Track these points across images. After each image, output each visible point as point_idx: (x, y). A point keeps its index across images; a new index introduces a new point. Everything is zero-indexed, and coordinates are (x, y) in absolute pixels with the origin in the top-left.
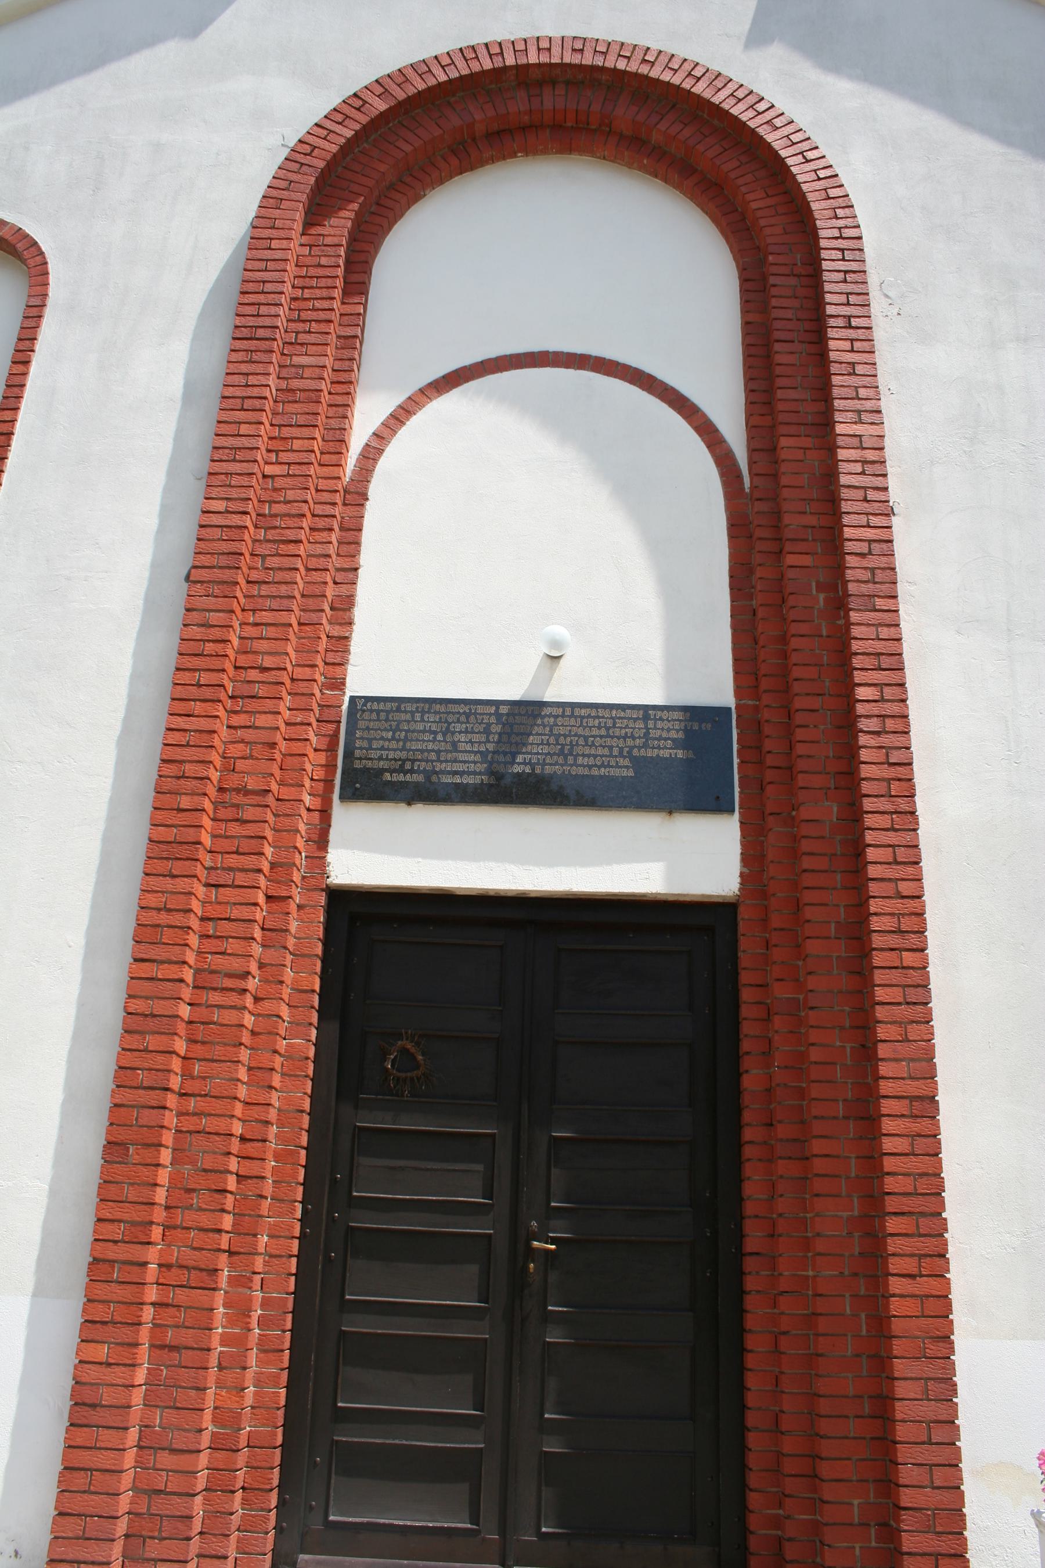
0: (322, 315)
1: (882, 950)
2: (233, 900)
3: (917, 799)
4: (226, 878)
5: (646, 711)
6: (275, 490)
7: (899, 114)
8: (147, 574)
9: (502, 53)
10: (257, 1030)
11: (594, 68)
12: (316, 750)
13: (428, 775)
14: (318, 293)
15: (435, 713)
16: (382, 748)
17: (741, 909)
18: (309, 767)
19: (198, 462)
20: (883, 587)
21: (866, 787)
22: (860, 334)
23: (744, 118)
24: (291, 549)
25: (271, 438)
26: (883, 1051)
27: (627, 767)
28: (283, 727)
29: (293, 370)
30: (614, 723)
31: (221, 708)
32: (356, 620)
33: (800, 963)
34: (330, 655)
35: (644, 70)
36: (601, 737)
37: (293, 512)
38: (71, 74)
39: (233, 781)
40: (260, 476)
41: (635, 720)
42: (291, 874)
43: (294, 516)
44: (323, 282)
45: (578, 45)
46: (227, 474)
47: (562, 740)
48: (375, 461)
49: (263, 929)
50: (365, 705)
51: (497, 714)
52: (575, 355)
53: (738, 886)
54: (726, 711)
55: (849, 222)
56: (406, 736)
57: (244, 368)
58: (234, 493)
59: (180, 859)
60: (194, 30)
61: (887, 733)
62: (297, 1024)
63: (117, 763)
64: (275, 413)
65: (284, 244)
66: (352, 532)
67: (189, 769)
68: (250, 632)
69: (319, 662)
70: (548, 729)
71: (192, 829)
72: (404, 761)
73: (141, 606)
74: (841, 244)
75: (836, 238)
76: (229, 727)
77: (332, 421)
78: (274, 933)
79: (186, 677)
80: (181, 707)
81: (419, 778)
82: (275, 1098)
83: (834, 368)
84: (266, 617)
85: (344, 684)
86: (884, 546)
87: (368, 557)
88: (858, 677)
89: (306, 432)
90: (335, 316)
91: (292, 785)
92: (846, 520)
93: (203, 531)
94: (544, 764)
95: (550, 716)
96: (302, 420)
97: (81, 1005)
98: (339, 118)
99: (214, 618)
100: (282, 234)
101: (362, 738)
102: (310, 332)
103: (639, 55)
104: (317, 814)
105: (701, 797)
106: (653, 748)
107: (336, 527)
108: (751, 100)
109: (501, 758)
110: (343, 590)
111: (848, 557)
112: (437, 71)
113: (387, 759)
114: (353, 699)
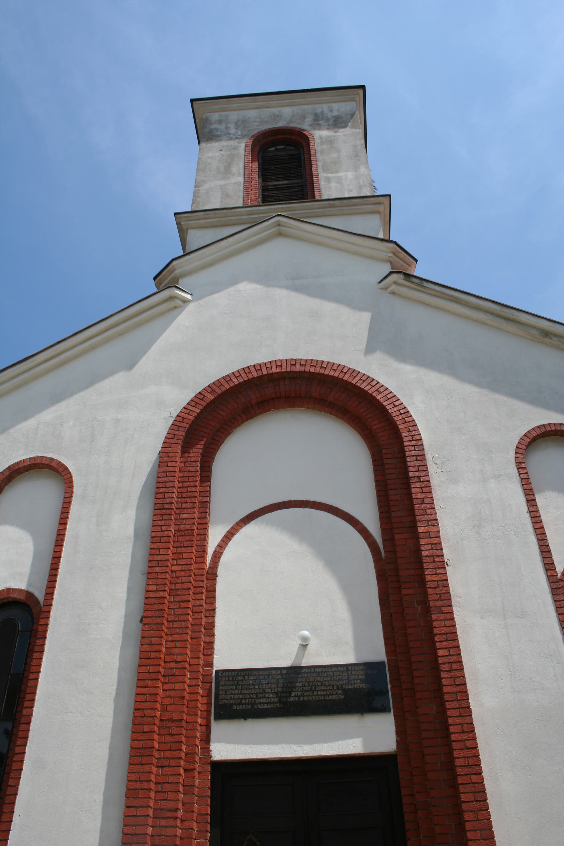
0: (192, 494)
1: (462, 775)
2: (169, 773)
3: (470, 700)
4: (166, 763)
5: (347, 667)
6: (177, 577)
7: (434, 379)
8: (123, 620)
9: (261, 369)
10: (183, 836)
11: (300, 372)
12: (202, 696)
13: (252, 705)
14: (189, 484)
15: (254, 675)
16: (232, 694)
17: (398, 758)
18: (199, 705)
19: (142, 566)
20: (445, 602)
21: (446, 697)
22: (425, 484)
23: (366, 389)
24: (186, 605)
25: (173, 553)
26: (468, 826)
27: (341, 694)
28: (187, 688)
29: (181, 521)
30: (334, 674)
31: (160, 683)
32: (216, 633)
33: (427, 783)
34: (205, 651)
35: (322, 371)
36: (328, 681)
37: (185, 587)
38: (79, 391)
39: (167, 716)
40: (170, 572)
41: (343, 671)
42: (194, 758)
43: (186, 589)
44: (191, 479)
45: (293, 363)
46: (155, 573)
47: (311, 684)
48: (219, 558)
49: (183, 786)
50: (222, 674)
51: (281, 674)
52: (303, 501)
53: (396, 747)
54: (382, 663)
55: (415, 433)
56: (242, 688)
57: (160, 523)
58: (159, 582)
59: (145, 756)
60: (130, 366)
61: (454, 670)
62: (201, 832)
63: (114, 710)
64: (174, 542)
65: (174, 464)
66: (212, 591)
67: (147, 712)
68: (170, 645)
69: (201, 656)
70: (304, 679)
71: (150, 741)
72: (242, 699)
73: (121, 635)
74: (413, 443)
75: (411, 441)
76: (163, 690)
77: (199, 542)
78: (189, 787)
79: (143, 669)
81: (249, 707)
83: (415, 502)
84: (176, 637)
85: (212, 664)
86: (444, 582)
87: (220, 604)
88: (438, 645)
89: (188, 550)
90: (197, 494)
91: (193, 715)
92: (426, 572)
93: (147, 600)
94: (304, 696)
95: (305, 673)
96: (186, 544)
97: (102, 831)
98: (194, 404)
99: (155, 641)
100: (172, 459)
101: (222, 690)
102: (187, 503)
103: (319, 365)
104: (204, 727)
106: (352, 684)
107: (204, 592)
108: (369, 380)
109: (285, 695)
110: (209, 620)
111: (429, 590)
112: (234, 379)
113: (234, 699)
114: (216, 671)
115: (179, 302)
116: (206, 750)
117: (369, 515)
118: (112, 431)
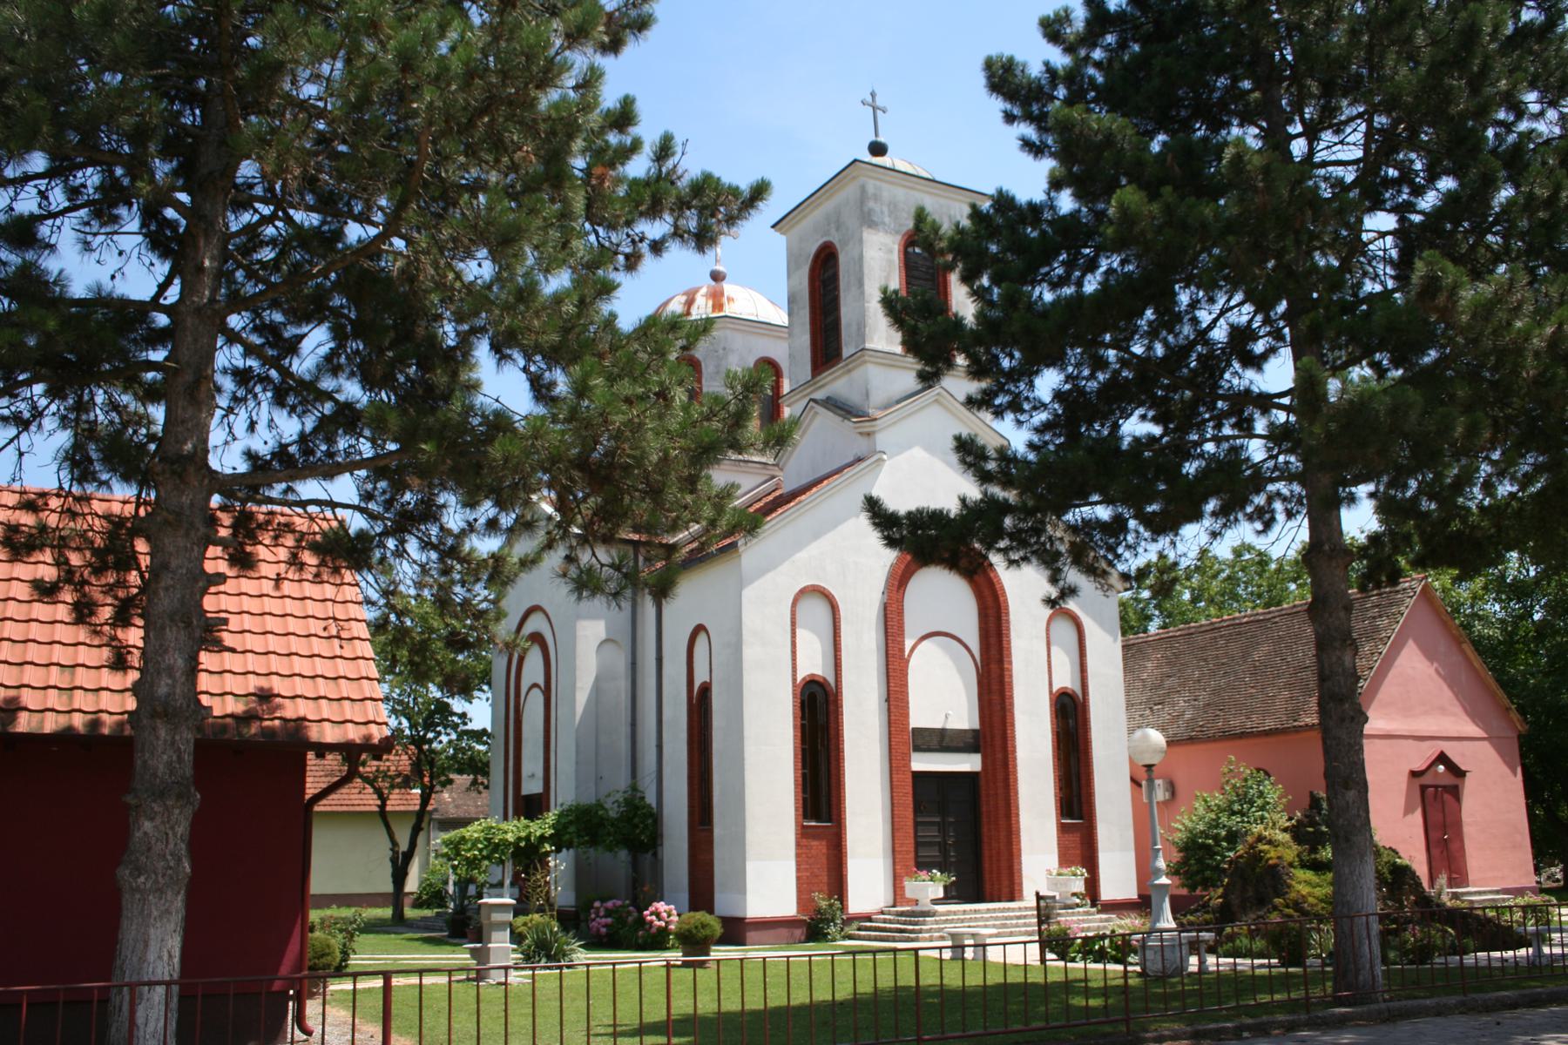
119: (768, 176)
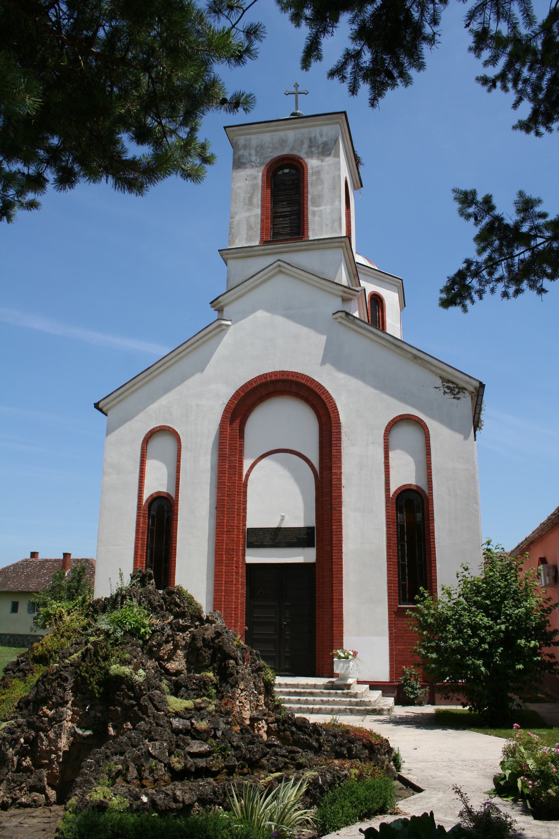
7: (355, 383)
19: (215, 483)
54: (313, 528)
60: (202, 370)
66: (245, 492)
67: (220, 547)
68: (228, 519)
78: (237, 573)
79: (218, 530)
80: (221, 450)
82: (239, 601)
84: (231, 516)
97: (207, 588)
99: (222, 518)
105: (309, 544)
115: (224, 327)
116: (244, 559)
117: (315, 460)
118: (196, 407)
119: (474, 78)
